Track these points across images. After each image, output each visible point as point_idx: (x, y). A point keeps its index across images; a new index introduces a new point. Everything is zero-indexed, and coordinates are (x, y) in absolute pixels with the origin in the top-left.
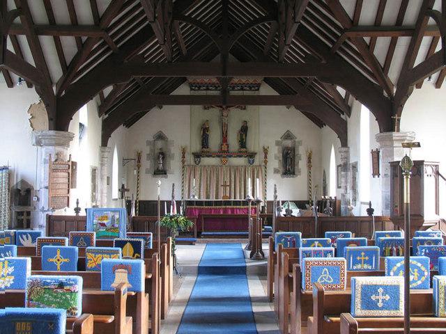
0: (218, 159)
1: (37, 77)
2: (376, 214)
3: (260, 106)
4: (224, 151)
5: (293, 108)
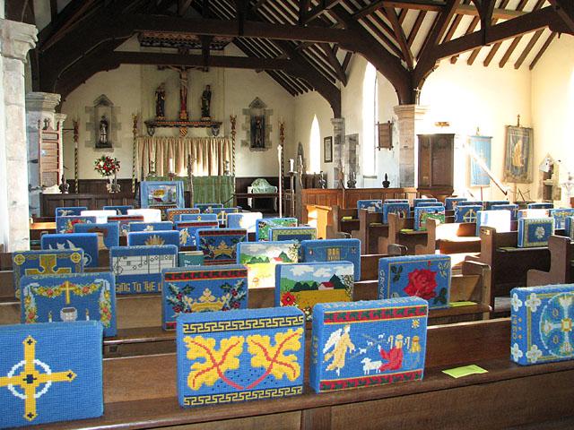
0: (176, 130)
2: (391, 186)
3: (226, 69)
4: (184, 120)
5: (122, 66)
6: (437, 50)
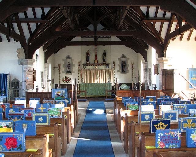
1: (20, 38)
3: (111, 46)
6: (170, 36)
